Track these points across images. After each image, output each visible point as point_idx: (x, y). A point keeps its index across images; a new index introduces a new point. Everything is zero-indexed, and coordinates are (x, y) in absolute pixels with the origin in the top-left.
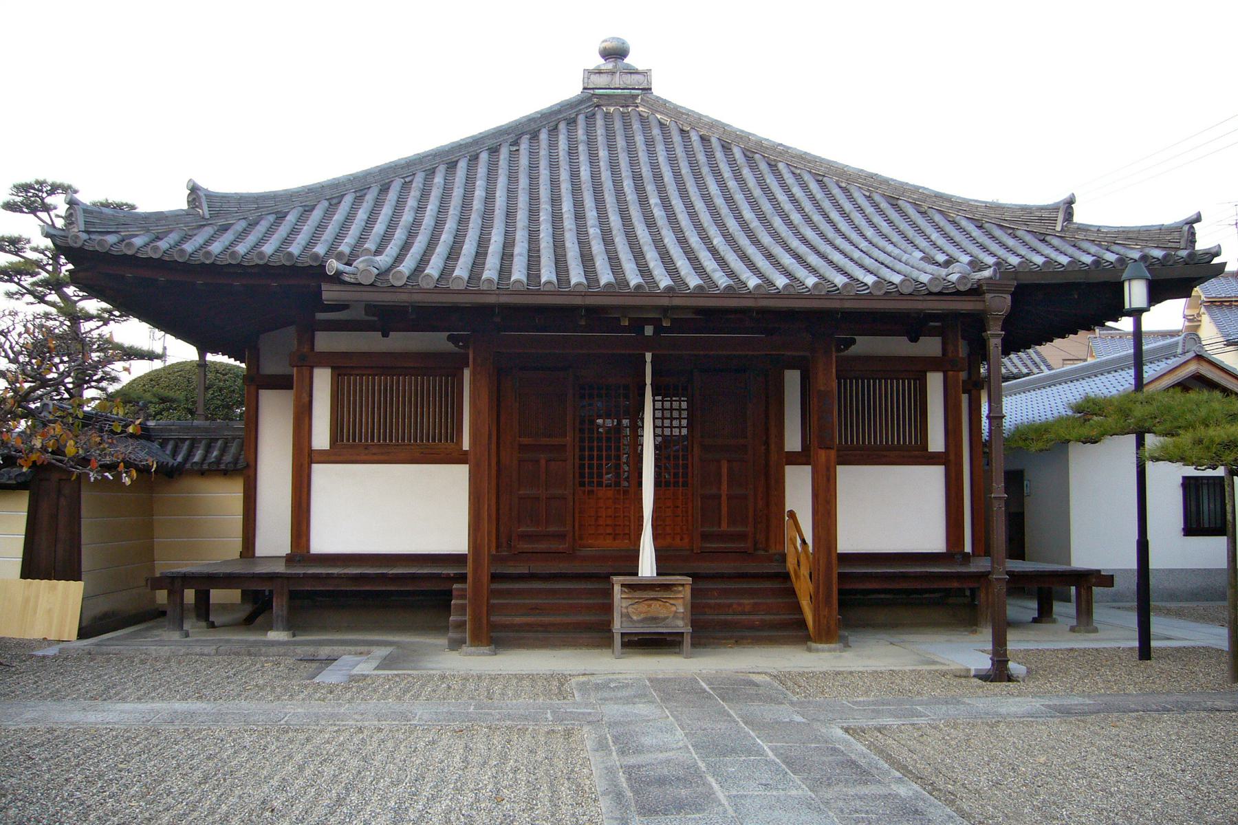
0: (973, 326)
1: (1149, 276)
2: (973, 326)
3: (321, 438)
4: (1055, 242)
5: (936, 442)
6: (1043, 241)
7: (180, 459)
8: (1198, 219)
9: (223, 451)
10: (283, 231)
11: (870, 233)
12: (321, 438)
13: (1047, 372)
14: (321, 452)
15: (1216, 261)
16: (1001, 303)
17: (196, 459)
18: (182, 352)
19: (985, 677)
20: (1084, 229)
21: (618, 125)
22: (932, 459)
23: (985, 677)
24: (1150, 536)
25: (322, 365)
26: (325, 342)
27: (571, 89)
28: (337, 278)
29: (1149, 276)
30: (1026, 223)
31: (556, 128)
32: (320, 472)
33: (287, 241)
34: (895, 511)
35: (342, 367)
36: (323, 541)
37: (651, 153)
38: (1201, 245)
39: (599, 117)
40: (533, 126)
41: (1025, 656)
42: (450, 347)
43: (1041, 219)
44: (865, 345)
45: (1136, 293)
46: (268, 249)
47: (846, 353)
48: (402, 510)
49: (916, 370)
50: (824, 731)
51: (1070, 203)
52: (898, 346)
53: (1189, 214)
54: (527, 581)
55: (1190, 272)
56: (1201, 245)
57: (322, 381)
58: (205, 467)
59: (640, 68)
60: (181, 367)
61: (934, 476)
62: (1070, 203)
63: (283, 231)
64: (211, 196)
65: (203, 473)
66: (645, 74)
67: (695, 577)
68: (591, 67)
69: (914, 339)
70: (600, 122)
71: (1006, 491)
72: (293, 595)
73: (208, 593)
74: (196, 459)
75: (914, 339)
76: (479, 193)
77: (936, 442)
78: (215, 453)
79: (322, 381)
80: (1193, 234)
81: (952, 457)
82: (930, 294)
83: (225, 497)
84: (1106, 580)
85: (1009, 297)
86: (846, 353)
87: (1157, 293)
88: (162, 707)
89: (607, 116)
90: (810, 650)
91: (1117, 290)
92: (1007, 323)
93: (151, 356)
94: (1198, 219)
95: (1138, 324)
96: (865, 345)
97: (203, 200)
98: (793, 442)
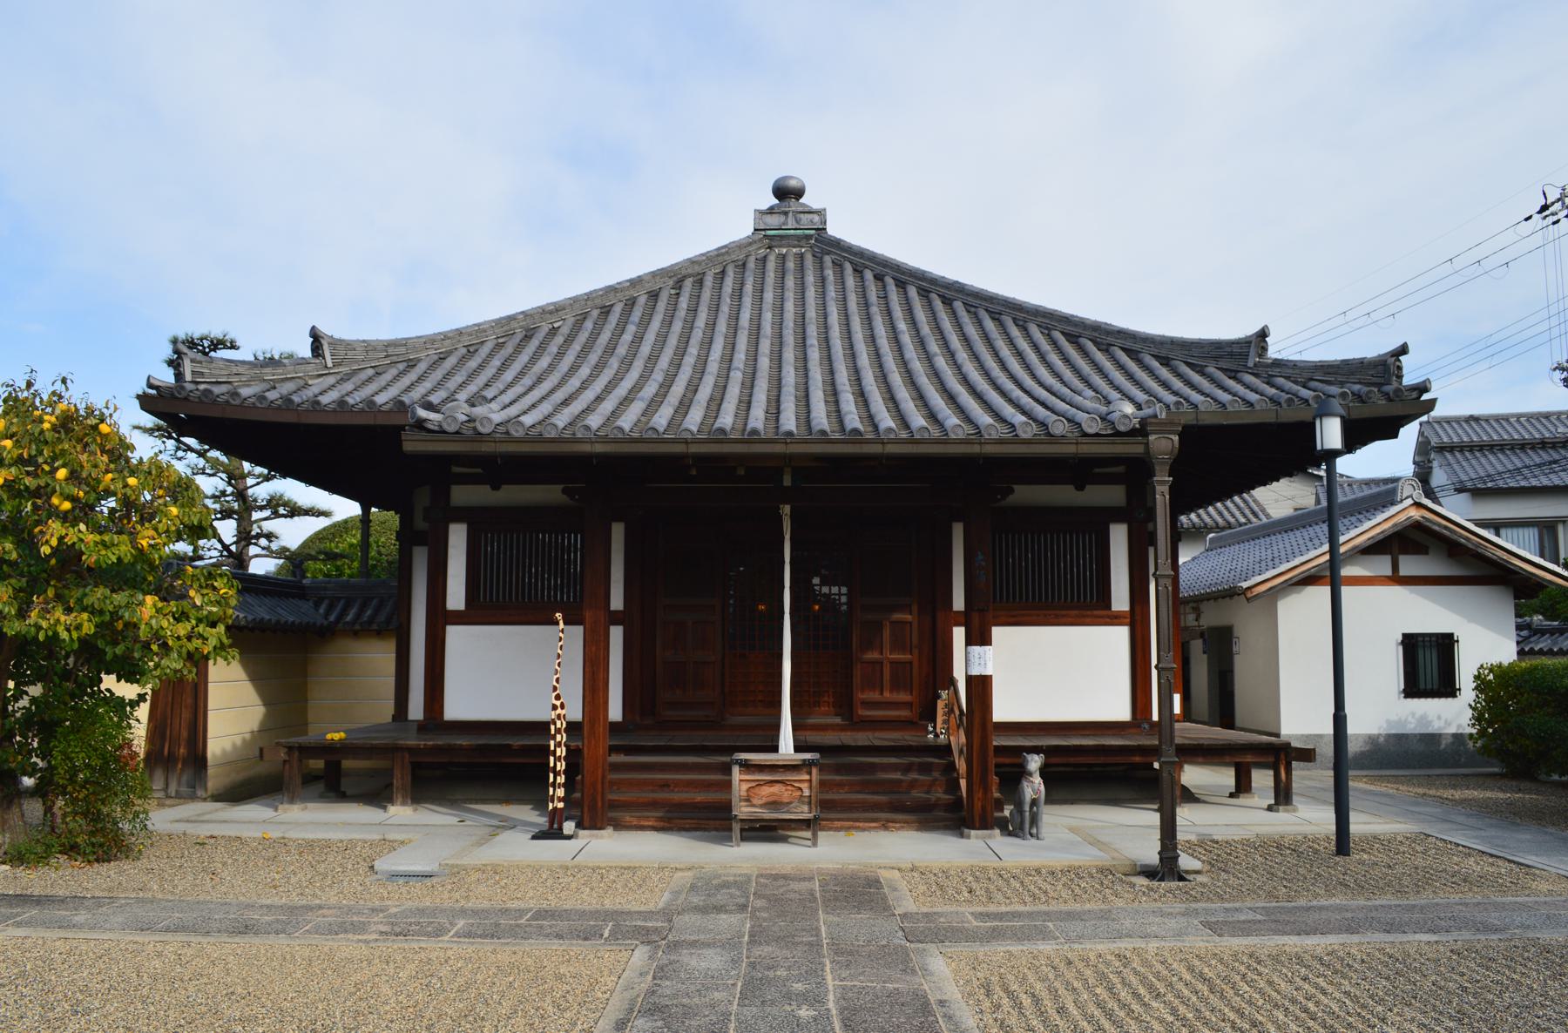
0: (1136, 472)
1: (1343, 412)
2: (1136, 472)
3: (456, 598)
4: (1249, 378)
5: (1120, 599)
6: (1234, 378)
7: (332, 618)
8: (1403, 350)
9: (377, 611)
10: (406, 381)
11: (1043, 372)
12: (456, 598)
13: (1265, 520)
14: (456, 613)
15: (1425, 397)
16: (1164, 445)
17: (349, 618)
18: (345, 508)
19: (1150, 873)
20: (1278, 363)
21: (791, 265)
22: (1114, 619)
23: (1150, 873)
24: (1348, 709)
25: (458, 520)
26: (462, 495)
27: (742, 229)
28: (420, 424)
29: (1343, 412)
30: (1216, 358)
31: (723, 272)
32: (457, 637)
33: (615, 414)
34: (1057, 674)
35: (481, 523)
36: (455, 710)
37: (822, 294)
38: (1409, 379)
39: (772, 258)
40: (697, 269)
41: (1205, 845)
42: (564, 499)
43: (1231, 355)
44: (1026, 494)
45: (1331, 433)
46: (627, 422)
47: (1003, 503)
48: (512, 674)
49: (1095, 524)
50: (693, 963)
51: (1263, 334)
52: (1062, 495)
53: (1394, 344)
54: (659, 751)
55: (1397, 410)
56: (1409, 379)
57: (458, 538)
58: (357, 627)
59: (815, 206)
60: (345, 526)
61: (1119, 636)
62: (1263, 334)
63: (406, 381)
64: (335, 343)
65: (356, 634)
66: (821, 213)
67: (1278, 735)
68: (765, 207)
69: (1080, 488)
70: (771, 265)
71: (1202, 655)
72: (416, 766)
73: (339, 763)
74: (349, 618)
75: (1080, 488)
76: (740, 357)
77: (1120, 599)
78: (369, 612)
79: (458, 538)
80: (1400, 368)
81: (1138, 617)
82: (1118, 434)
83: (379, 658)
84: (1307, 755)
85: (1176, 438)
86: (1003, 503)
87: (1356, 436)
88: (1489, 794)
89: (783, 258)
90: (962, 836)
91: (1307, 431)
92: (1178, 467)
93: (326, 514)
94: (1403, 350)
95: (1331, 471)
96: (1026, 494)
97: (326, 347)
98: (959, 603)
